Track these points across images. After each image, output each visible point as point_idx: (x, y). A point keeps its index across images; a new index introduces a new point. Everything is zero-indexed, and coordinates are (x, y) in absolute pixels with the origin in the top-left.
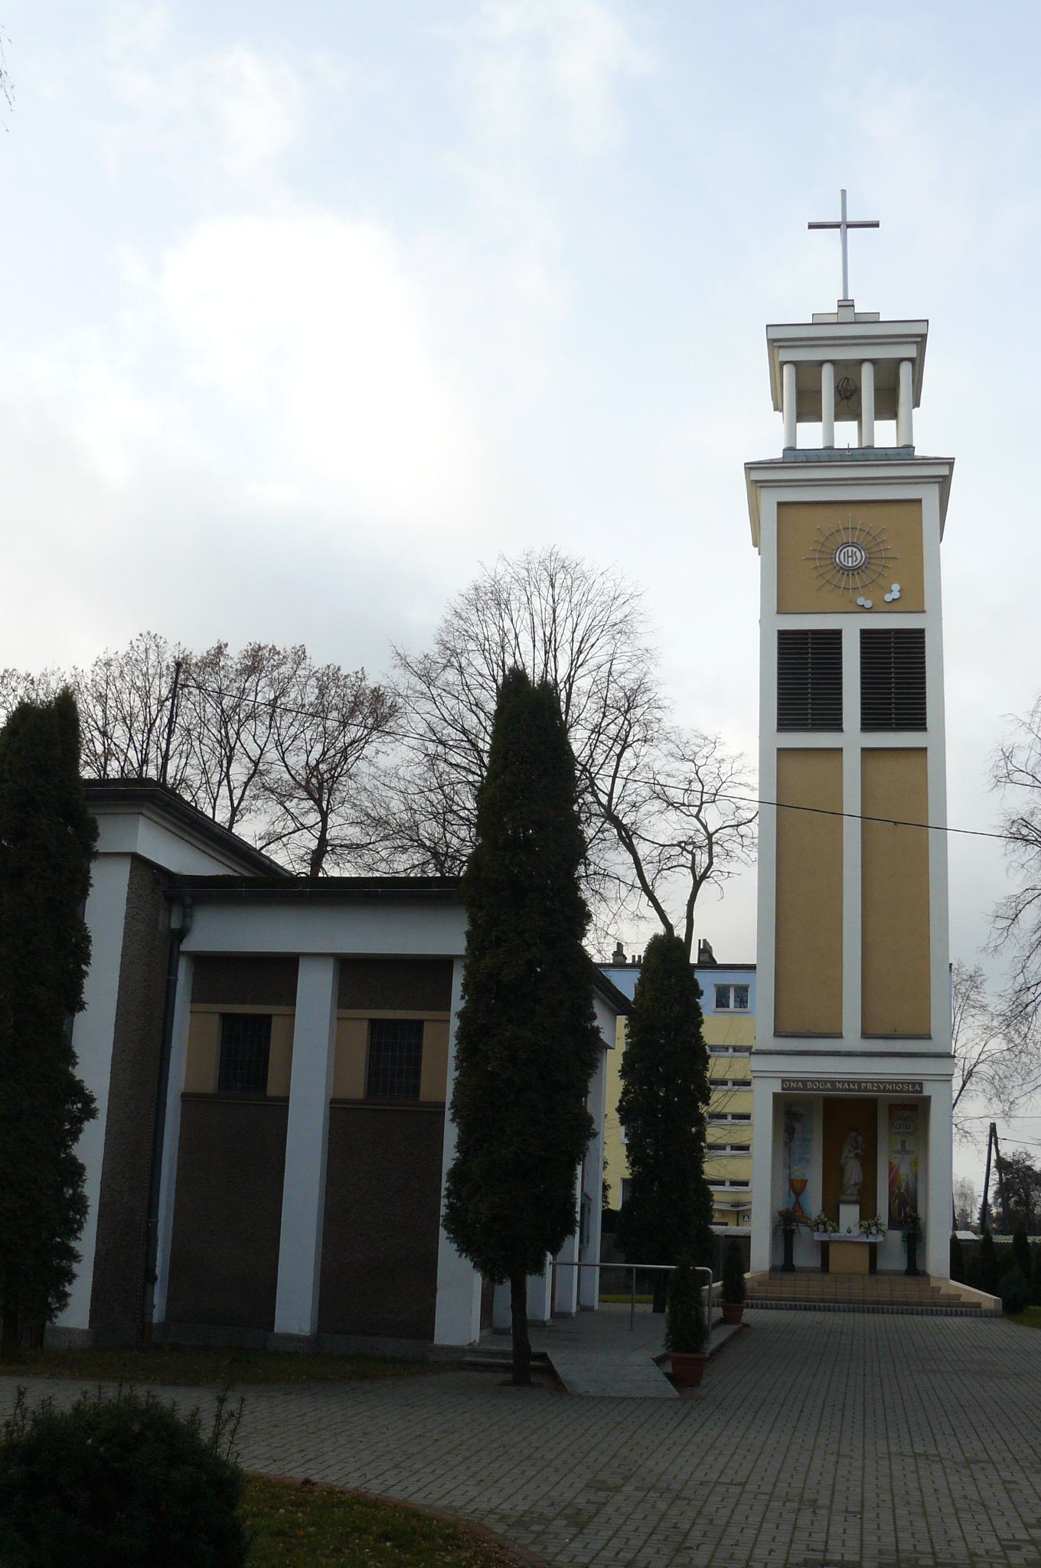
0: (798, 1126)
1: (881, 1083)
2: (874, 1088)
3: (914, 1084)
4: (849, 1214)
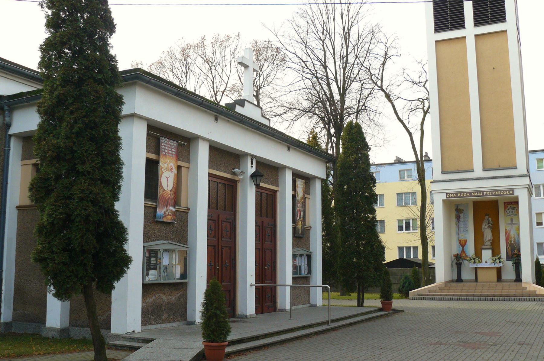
0: (461, 215)
1: (494, 191)
3: (509, 191)
4: (487, 254)
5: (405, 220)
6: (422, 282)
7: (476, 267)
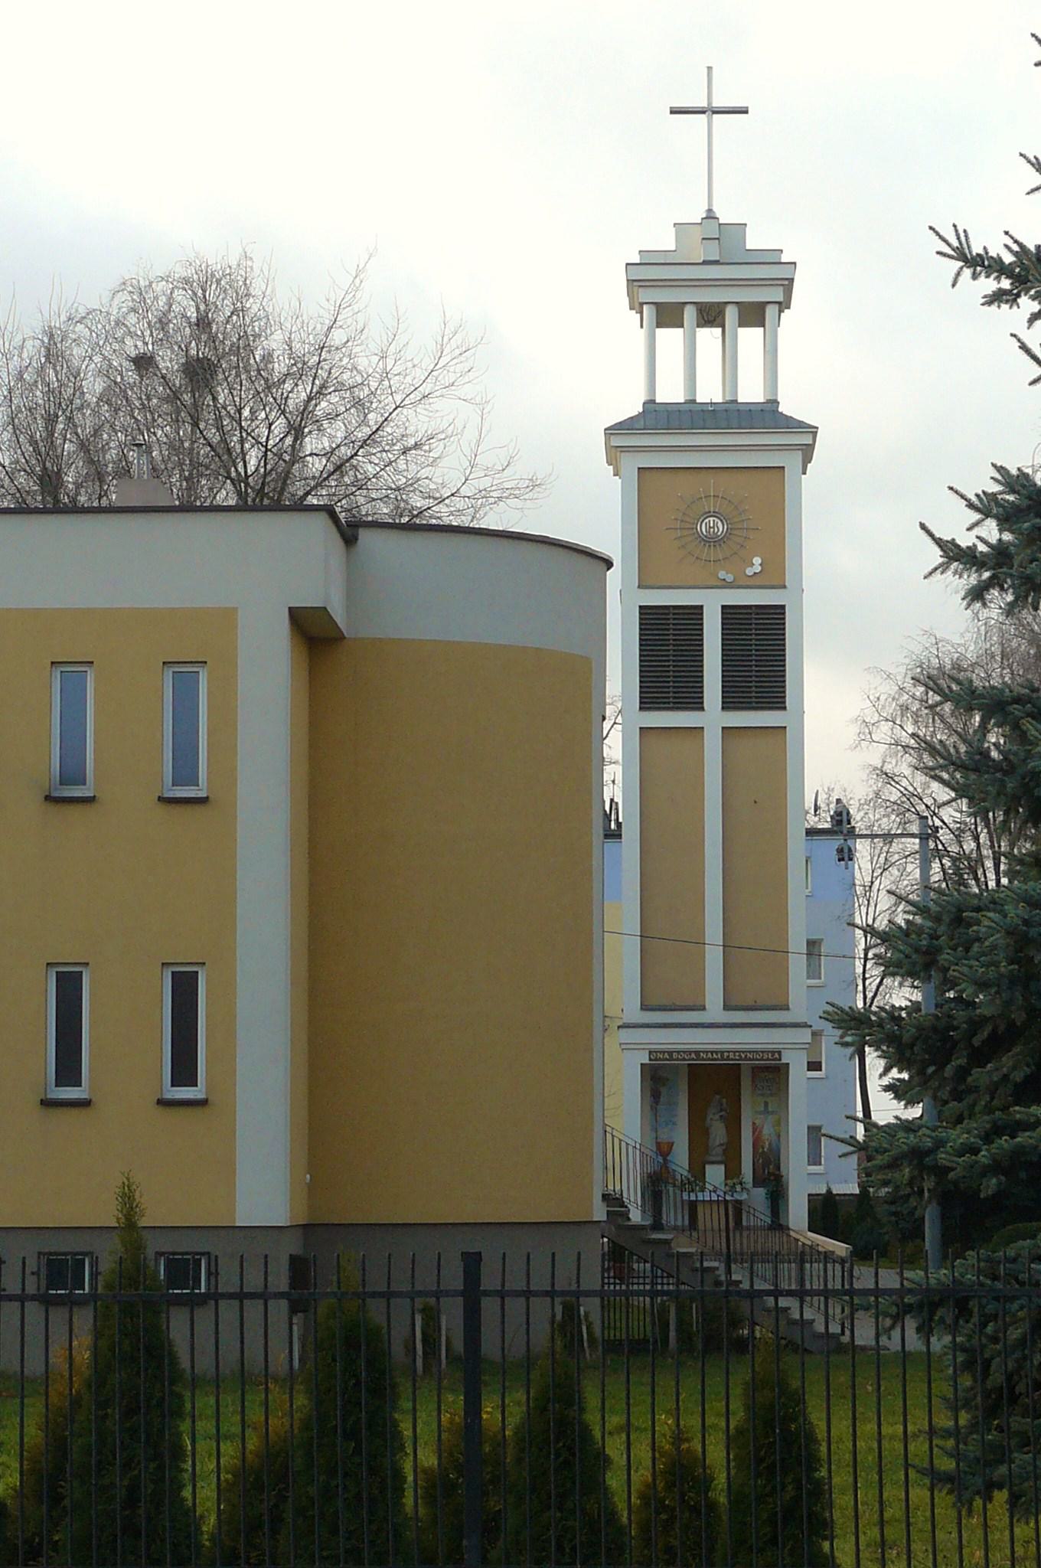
0: (664, 1091)
1: (743, 1052)
3: (773, 1053)
4: (715, 1174)
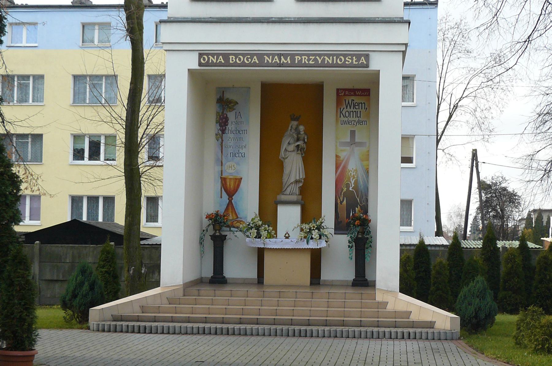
0: (231, 116)
1: (320, 56)
2: (311, 62)
3: (359, 57)
5: (90, 136)
6: (123, 279)
7: (262, 246)
